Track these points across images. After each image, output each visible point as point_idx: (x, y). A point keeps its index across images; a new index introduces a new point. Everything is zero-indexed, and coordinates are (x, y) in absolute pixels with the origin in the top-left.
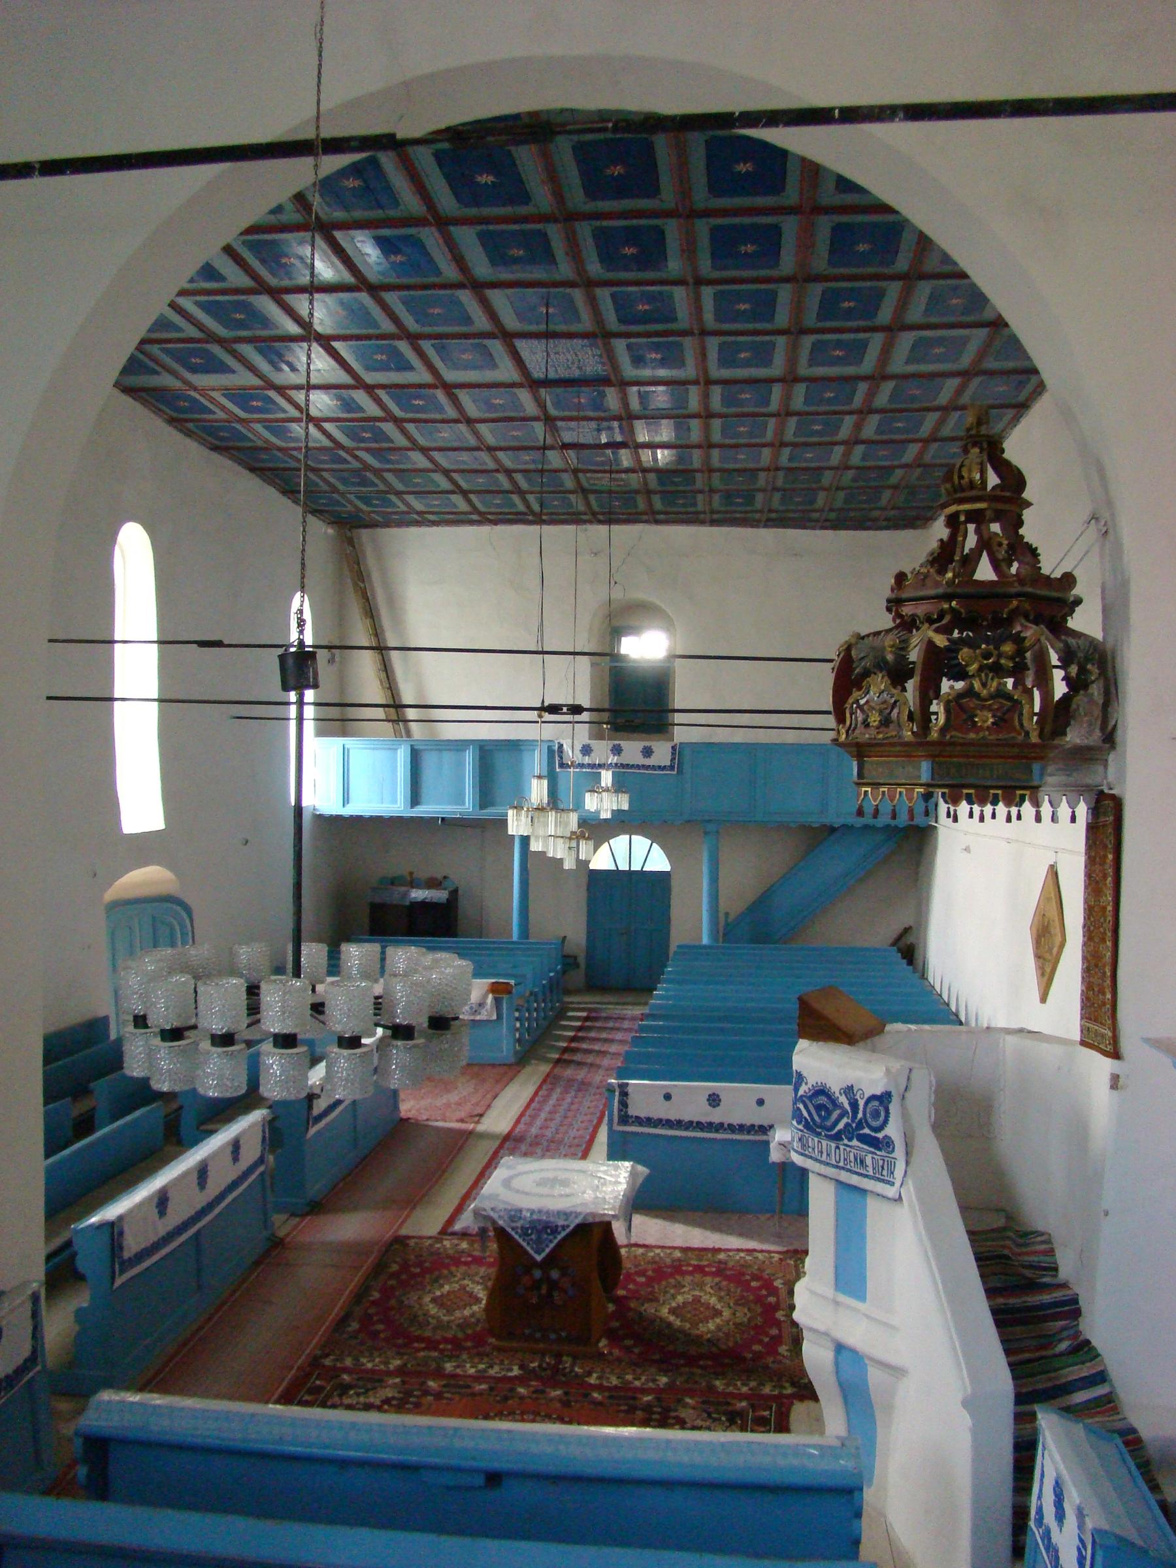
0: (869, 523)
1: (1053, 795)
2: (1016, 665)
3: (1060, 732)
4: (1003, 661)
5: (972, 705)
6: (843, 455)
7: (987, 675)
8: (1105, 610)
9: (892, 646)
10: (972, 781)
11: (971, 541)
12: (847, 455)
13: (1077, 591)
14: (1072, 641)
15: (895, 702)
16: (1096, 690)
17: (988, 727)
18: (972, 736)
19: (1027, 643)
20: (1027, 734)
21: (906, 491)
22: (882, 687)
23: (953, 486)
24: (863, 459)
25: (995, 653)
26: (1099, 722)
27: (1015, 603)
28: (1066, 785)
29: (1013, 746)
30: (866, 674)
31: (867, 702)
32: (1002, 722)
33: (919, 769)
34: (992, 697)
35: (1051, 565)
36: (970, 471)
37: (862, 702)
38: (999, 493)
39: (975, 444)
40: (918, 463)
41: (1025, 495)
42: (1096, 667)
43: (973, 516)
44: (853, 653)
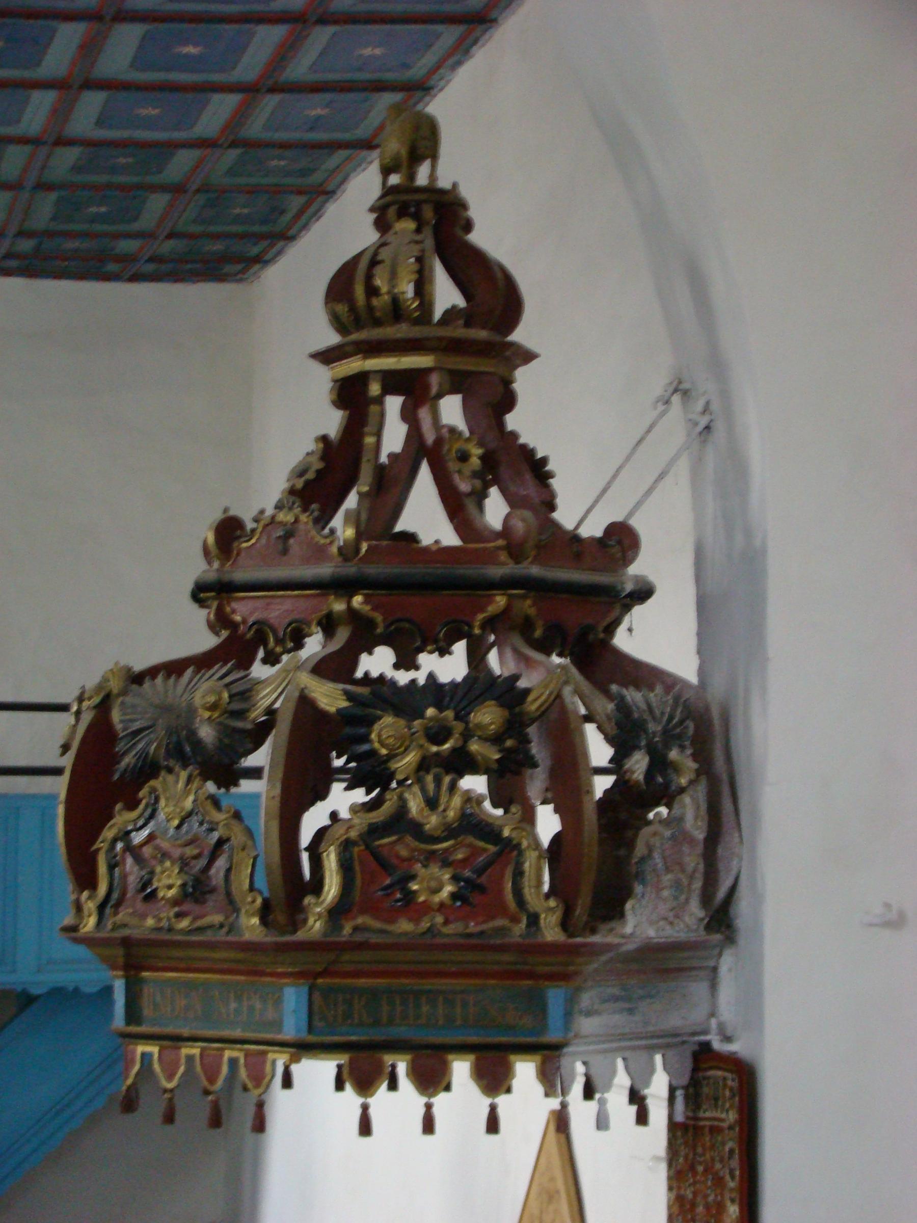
0: (112, 267)
1: (598, 1063)
2: (508, 753)
3: (610, 905)
4: (474, 747)
5: (404, 853)
6: (54, 111)
7: (438, 781)
8: (703, 606)
9: (213, 707)
10: (400, 1032)
11: (394, 437)
12: (61, 113)
13: (639, 568)
14: (633, 696)
15: (221, 842)
16: (691, 810)
17: (442, 905)
18: (404, 926)
19: (532, 706)
20: (534, 920)
21: (201, 199)
22: (188, 803)
23: (353, 309)
24: (100, 122)
25: (459, 727)
26: (698, 884)
27: (501, 601)
28: (623, 1037)
29: (502, 948)
30: (149, 769)
31: (151, 838)
32: (472, 893)
33: (278, 1002)
34: (451, 832)
35: (579, 510)
36: (393, 276)
37: (138, 838)
38: (459, 331)
39: (402, 213)
40: (231, 137)
41: (518, 336)
42: (688, 748)
43: (395, 382)
44: (116, 716)
